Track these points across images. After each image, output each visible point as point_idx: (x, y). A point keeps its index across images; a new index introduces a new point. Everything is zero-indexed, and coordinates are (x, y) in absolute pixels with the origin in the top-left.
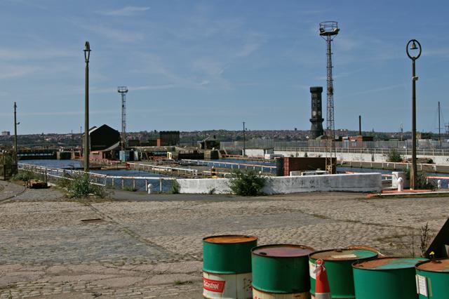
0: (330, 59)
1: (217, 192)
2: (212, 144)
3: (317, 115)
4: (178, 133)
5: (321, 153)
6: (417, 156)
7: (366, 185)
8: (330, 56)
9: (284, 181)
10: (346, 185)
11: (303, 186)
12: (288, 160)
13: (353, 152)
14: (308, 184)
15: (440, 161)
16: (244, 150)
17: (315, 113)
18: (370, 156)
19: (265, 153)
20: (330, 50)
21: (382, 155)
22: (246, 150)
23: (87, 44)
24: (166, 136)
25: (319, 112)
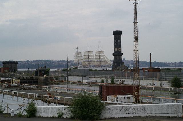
0: (136, 16)
1: (65, 116)
2: (43, 72)
3: (118, 50)
4: (16, 63)
5: (124, 80)
6: (89, 58)
7: (172, 111)
8: (136, 15)
9: (114, 108)
10: (158, 112)
11: (128, 113)
12: (105, 88)
13: (147, 80)
14: (131, 111)
15: (182, 80)
16: (67, 76)
17: (116, 50)
18: (159, 82)
19: (83, 79)
20: (136, 10)
21: (167, 82)
22: (69, 77)
23: (151, 53)
24: (7, 65)
25: (119, 49)
